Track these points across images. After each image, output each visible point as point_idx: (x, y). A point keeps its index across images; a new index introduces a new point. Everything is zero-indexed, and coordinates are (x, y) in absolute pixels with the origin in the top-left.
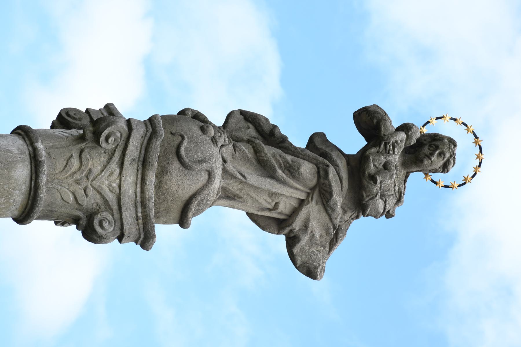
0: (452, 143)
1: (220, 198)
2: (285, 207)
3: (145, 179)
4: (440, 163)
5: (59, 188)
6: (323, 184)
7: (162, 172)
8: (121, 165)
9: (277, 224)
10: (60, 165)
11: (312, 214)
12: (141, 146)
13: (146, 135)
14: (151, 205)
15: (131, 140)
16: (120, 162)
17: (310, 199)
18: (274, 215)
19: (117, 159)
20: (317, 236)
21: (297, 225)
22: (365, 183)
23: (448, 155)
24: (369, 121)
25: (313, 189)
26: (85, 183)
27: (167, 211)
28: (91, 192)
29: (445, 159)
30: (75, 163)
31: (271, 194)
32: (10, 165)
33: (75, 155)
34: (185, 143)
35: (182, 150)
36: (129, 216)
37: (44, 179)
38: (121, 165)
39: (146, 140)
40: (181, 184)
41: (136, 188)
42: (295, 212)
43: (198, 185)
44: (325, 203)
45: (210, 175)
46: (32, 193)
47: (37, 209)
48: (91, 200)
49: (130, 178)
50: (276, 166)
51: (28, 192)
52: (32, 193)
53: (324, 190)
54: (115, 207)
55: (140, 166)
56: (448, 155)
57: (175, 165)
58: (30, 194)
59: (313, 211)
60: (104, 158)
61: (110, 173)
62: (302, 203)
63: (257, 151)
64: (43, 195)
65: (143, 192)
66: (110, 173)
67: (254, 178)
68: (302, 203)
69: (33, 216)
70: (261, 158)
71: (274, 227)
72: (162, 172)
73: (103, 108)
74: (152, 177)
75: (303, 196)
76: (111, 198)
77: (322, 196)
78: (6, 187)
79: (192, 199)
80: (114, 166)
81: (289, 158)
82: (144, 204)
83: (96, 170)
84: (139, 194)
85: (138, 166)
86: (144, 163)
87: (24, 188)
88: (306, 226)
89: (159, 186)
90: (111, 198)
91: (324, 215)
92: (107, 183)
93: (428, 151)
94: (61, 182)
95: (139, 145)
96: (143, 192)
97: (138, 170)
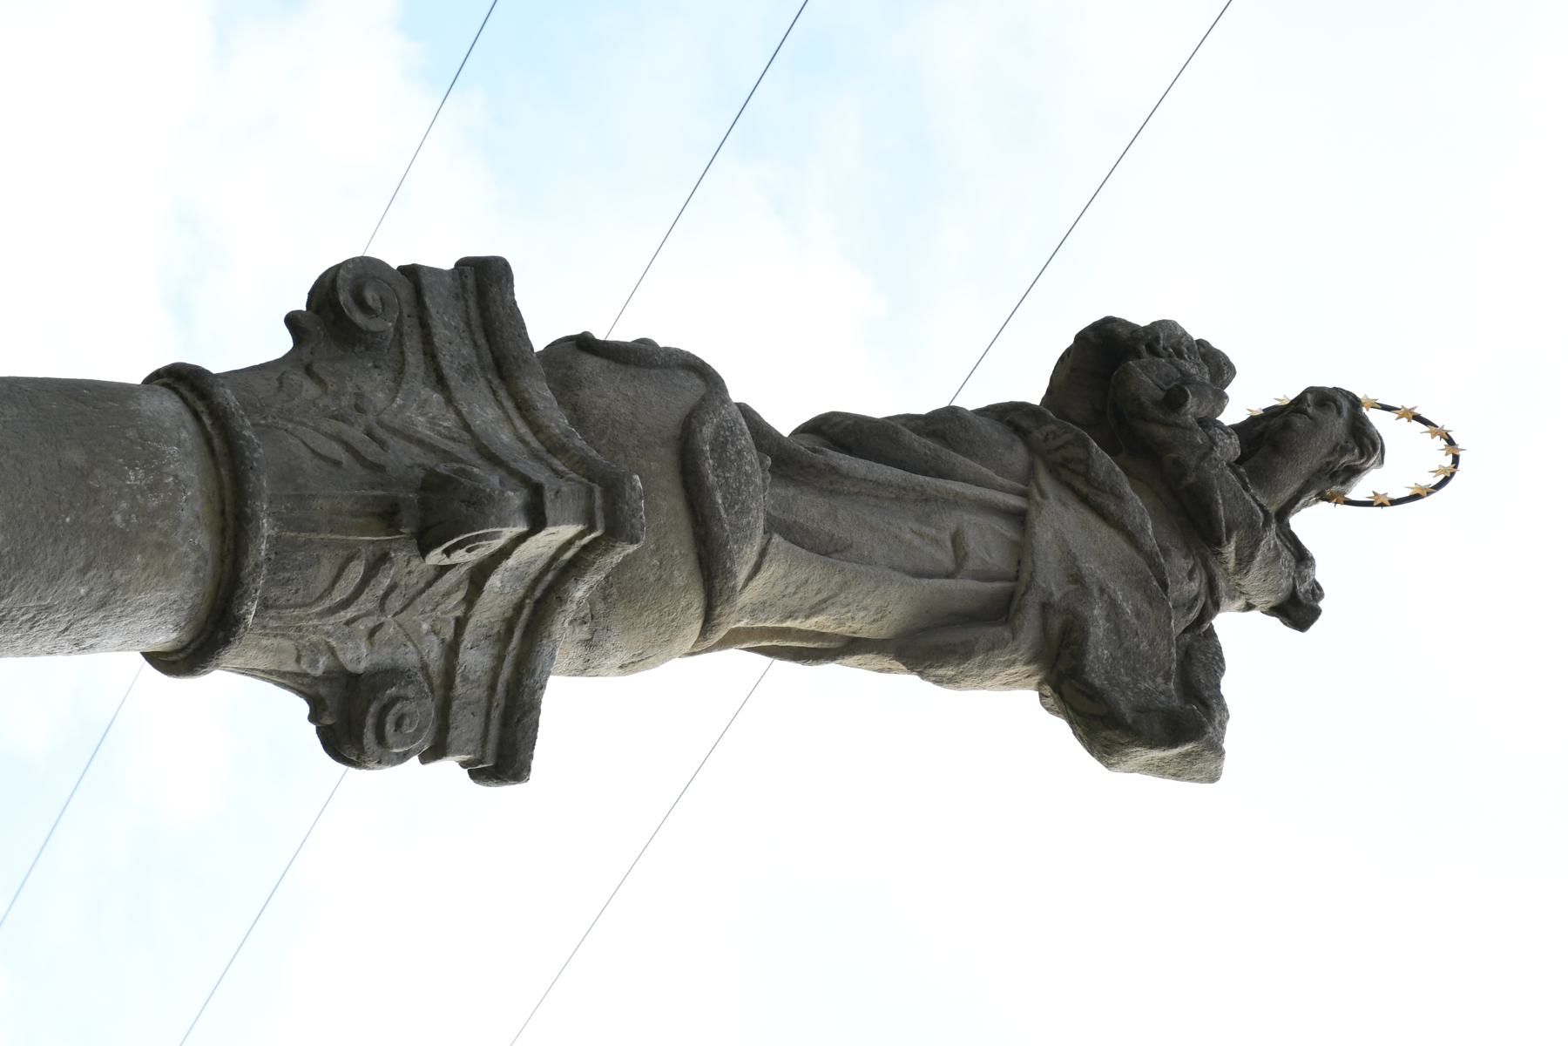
3: (525, 400)
5: (290, 426)
6: (1046, 439)
11: (1069, 537)
12: (468, 325)
13: (464, 286)
15: (427, 300)
16: (433, 379)
17: (1038, 498)
19: (421, 372)
22: (1162, 433)
25: (1030, 475)
29: (1345, 413)
39: (472, 303)
41: (515, 429)
42: (1022, 550)
44: (1085, 489)
46: (217, 442)
47: (251, 475)
51: (205, 448)
52: (217, 442)
53: (1058, 449)
55: (496, 382)
58: (212, 452)
61: (410, 503)
65: (536, 428)
66: (410, 503)
69: (255, 513)
77: (1064, 473)
78: (131, 433)
79: (690, 423)
84: (530, 438)
85: (489, 382)
87: (188, 434)
88: (1077, 578)
91: (1104, 532)
95: (462, 325)
96: (536, 428)
97: (494, 393)
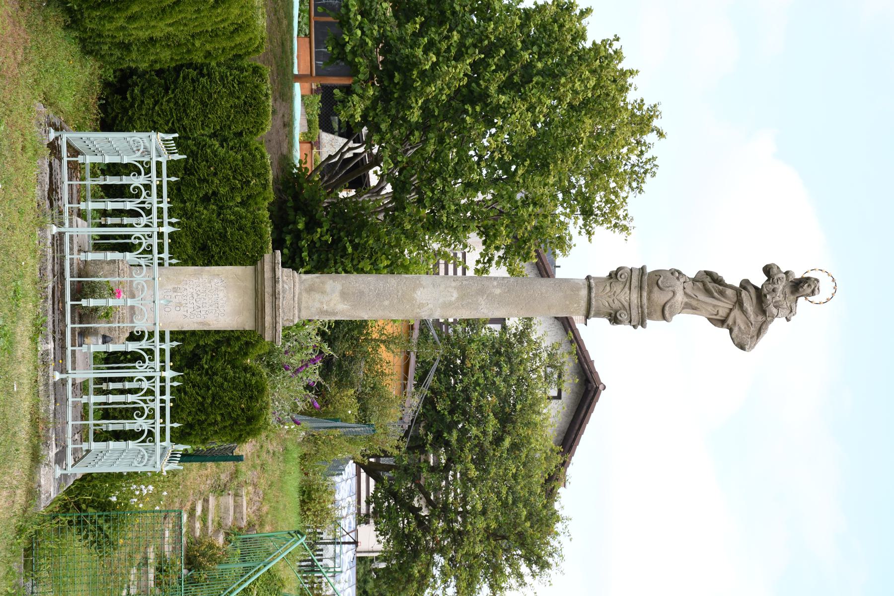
0: (817, 280)
1: (683, 308)
2: (723, 313)
4: (809, 291)
7: (650, 292)
8: (630, 289)
9: (721, 322)
10: (601, 289)
14: (645, 307)
18: (718, 317)
20: (743, 328)
21: (730, 321)
23: (813, 287)
24: (767, 270)
26: (613, 297)
27: (655, 311)
28: (616, 302)
30: (608, 288)
31: (714, 306)
32: (579, 289)
33: (608, 285)
34: (661, 279)
35: (660, 282)
36: (634, 313)
37: (593, 295)
38: (630, 289)
40: (660, 297)
42: (728, 315)
43: (669, 298)
45: (674, 293)
48: (617, 305)
49: (635, 296)
50: (271, 172)
54: (628, 308)
56: (813, 287)
57: (656, 289)
59: (736, 313)
60: (622, 286)
62: (731, 310)
63: (704, 285)
64: (593, 302)
67: (702, 297)
68: (731, 310)
70: (280, 177)
71: (720, 324)
72: (650, 292)
73: (691, 272)
74: (645, 294)
75: (731, 307)
76: (626, 305)
80: (627, 289)
81: (721, 288)
82: (641, 307)
83: (618, 292)
86: (641, 288)
87: (586, 299)
88: (735, 322)
89: (649, 299)
90: (626, 305)
92: (624, 297)
93: (801, 286)
94: (601, 297)
